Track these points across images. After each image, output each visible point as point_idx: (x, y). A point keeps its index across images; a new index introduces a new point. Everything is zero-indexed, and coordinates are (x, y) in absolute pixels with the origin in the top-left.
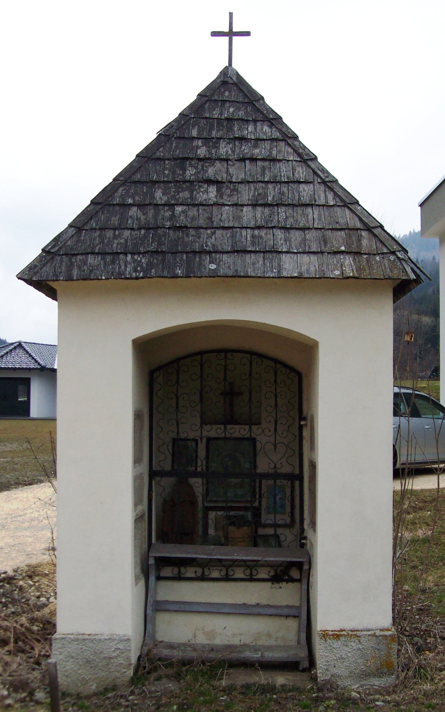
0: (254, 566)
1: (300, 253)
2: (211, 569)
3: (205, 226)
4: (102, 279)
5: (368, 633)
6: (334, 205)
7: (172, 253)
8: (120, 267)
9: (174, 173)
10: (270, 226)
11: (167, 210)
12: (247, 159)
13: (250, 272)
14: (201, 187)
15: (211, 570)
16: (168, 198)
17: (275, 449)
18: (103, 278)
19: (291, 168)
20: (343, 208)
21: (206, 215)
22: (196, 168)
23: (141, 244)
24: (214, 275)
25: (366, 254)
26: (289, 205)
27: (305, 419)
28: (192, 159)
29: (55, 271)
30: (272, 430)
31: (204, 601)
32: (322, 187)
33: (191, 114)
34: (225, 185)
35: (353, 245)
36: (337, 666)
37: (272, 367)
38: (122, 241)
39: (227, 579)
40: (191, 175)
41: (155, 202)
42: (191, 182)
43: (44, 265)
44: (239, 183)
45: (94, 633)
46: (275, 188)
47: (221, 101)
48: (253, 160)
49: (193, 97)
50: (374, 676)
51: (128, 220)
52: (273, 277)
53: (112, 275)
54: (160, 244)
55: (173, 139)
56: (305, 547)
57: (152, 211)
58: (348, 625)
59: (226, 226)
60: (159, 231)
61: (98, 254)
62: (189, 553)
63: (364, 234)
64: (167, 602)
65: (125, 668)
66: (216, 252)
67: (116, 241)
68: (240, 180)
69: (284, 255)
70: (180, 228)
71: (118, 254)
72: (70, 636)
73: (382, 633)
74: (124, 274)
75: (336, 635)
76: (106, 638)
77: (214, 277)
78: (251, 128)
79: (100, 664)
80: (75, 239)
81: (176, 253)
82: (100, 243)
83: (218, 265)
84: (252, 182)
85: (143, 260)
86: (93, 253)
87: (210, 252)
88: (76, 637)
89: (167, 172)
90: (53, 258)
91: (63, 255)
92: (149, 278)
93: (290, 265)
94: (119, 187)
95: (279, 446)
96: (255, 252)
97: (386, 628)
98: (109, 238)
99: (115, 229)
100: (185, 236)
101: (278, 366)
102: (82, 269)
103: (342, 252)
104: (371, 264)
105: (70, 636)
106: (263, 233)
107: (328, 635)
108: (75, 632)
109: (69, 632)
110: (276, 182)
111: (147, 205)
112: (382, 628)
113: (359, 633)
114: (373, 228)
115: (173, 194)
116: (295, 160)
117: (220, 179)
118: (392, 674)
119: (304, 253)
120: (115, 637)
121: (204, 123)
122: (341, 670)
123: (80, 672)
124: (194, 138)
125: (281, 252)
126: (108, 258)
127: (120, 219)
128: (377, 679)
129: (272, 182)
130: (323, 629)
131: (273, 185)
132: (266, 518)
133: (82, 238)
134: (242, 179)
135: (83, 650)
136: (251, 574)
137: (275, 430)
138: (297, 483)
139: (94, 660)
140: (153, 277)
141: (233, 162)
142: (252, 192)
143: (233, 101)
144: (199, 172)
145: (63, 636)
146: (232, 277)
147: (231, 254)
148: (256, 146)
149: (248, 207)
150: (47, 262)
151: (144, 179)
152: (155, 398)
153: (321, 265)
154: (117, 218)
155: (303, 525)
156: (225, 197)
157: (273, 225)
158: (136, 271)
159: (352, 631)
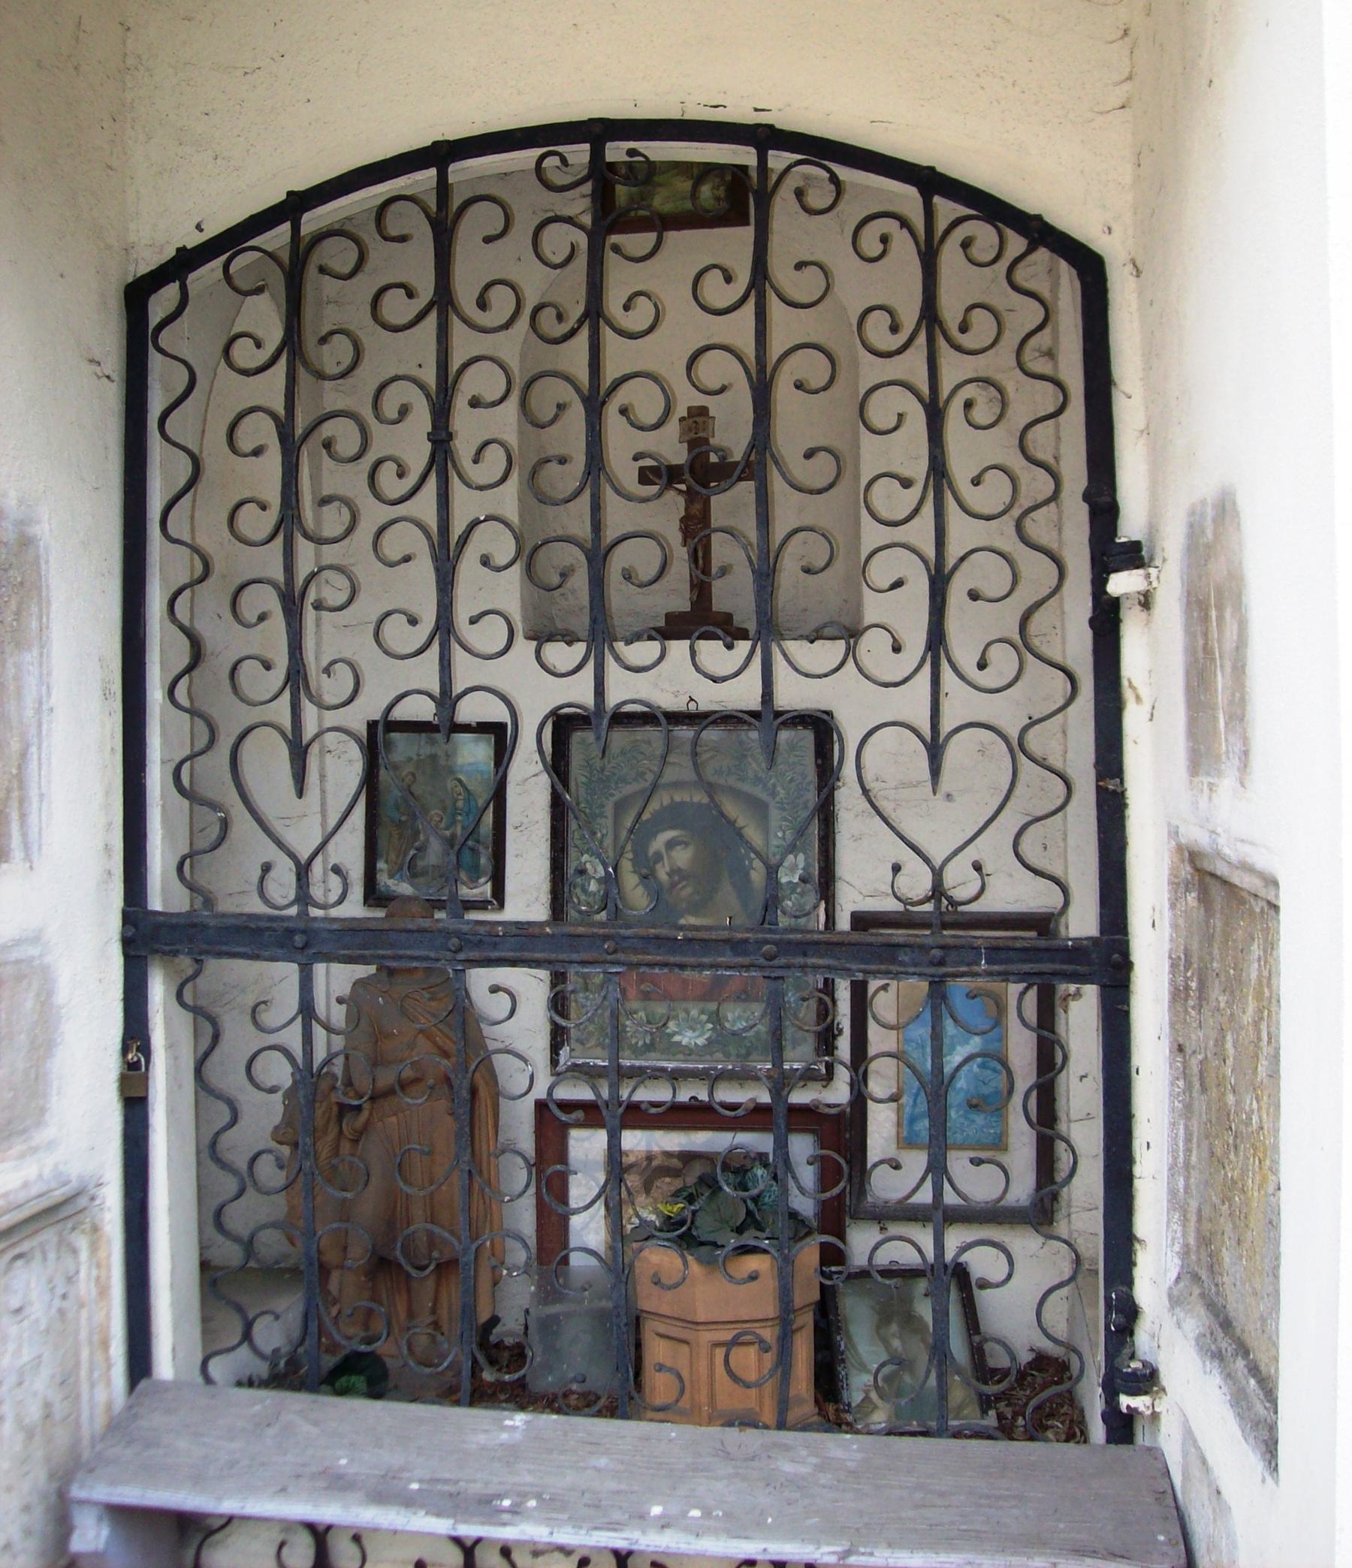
17: (935, 771)
27: (1134, 556)
30: (916, 641)
37: (905, 223)
56: (1142, 1438)
95: (955, 753)
101: (947, 209)
132: (896, 1172)
137: (936, 640)
138: (1081, 1015)
152: (155, 445)
155: (1130, 1282)
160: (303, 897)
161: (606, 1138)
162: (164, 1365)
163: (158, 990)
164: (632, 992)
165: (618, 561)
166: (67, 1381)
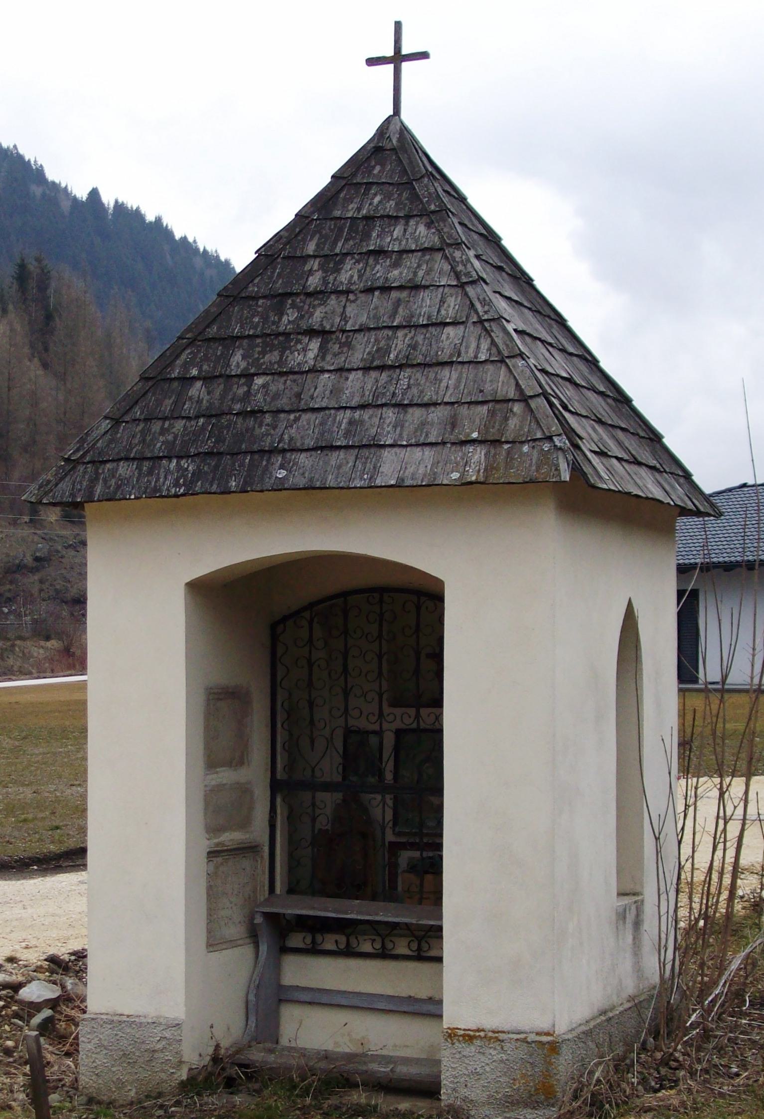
0: (424, 937)
1: (411, 445)
2: (360, 938)
3: (287, 409)
4: (130, 499)
5: (518, 1036)
6: (485, 361)
7: (233, 454)
8: (158, 480)
9: (265, 319)
10: (379, 403)
11: (243, 384)
12: (378, 288)
13: (331, 481)
14: (299, 341)
15: (360, 938)
16: (248, 364)
18: (133, 497)
19: (438, 300)
20: (499, 365)
21: (296, 389)
22: (300, 309)
23: (194, 441)
24: (280, 487)
25: (507, 442)
26: (419, 365)
28: (297, 294)
29: (73, 489)
31: (350, 990)
32: (478, 330)
33: (313, 213)
34: (334, 337)
35: (493, 427)
36: (469, 1085)
38: (170, 438)
39: (384, 955)
40: (289, 322)
41: (228, 372)
42: (286, 334)
43: (62, 479)
44: (355, 331)
45: (137, 1014)
46: (406, 335)
47: (366, 183)
48: (386, 289)
49: (325, 180)
50: (526, 1106)
51: (185, 404)
52: (361, 488)
53: (145, 492)
54: (220, 440)
55: (279, 260)
57: (222, 386)
58: (490, 1022)
59: (316, 406)
60: (224, 421)
61: (134, 459)
62: (314, 908)
63: (517, 408)
64: (297, 988)
65: (173, 1068)
66: (292, 450)
67: (161, 439)
68: (357, 327)
69: (387, 449)
70: (253, 412)
71: (161, 458)
72: (102, 1017)
73: (538, 1038)
74: (160, 490)
75: (469, 1035)
76: (150, 1021)
77: (280, 490)
78: (398, 232)
79: (141, 1060)
80: (108, 437)
81: (237, 454)
82: (140, 442)
83: (290, 471)
84: (374, 329)
85: (190, 468)
86: (127, 459)
87: (284, 451)
88: (109, 1017)
89: (256, 320)
90: (74, 468)
91: (88, 463)
92: (192, 494)
93: (389, 467)
94: (184, 349)
96: (347, 447)
97: (545, 1031)
98: (155, 432)
99: (165, 419)
100: (256, 426)
102: (109, 483)
103: (474, 441)
104: (512, 459)
105: (102, 1017)
106: (366, 414)
107: (455, 1035)
108: (110, 1011)
109: (103, 1011)
110: (410, 327)
111: (217, 377)
112: (539, 1030)
113: (502, 1036)
114: (531, 397)
115: (257, 356)
116: (449, 285)
117: (328, 328)
118: (553, 1106)
119: (417, 445)
120: (162, 1020)
121: (330, 228)
122: (476, 1093)
123: (114, 1069)
124: (309, 256)
125: (384, 446)
126: (146, 465)
127: (175, 403)
128: (530, 1111)
129: (405, 327)
130: (451, 1027)
131: (406, 331)
133: (119, 435)
134: (361, 325)
135: (118, 1037)
136: (419, 949)
139: (134, 1053)
140: (197, 494)
141: (356, 295)
142: (370, 346)
143: (383, 183)
144: (302, 317)
145: (94, 1016)
146: (305, 489)
147: (313, 453)
148: (396, 265)
149: (359, 372)
150: (66, 475)
151: (223, 334)
152: (279, 688)
153: (436, 464)
154: (171, 401)
156: (328, 358)
157: (384, 401)
158: (177, 484)
159: (494, 1032)
160: (313, 776)
161: (79, 196)
162: (278, 891)
163: (279, 800)
164: (562, 1082)
165: (376, 718)
166: (254, 891)
